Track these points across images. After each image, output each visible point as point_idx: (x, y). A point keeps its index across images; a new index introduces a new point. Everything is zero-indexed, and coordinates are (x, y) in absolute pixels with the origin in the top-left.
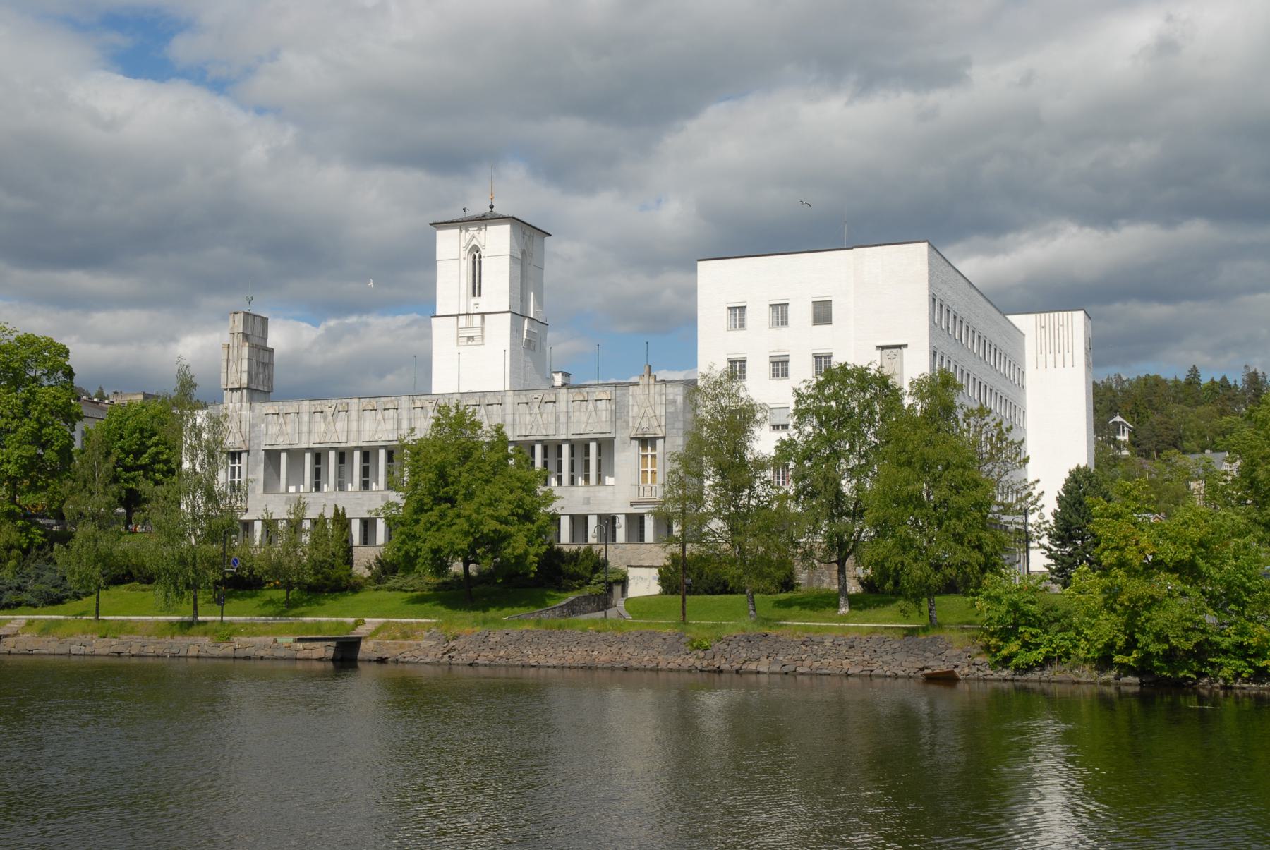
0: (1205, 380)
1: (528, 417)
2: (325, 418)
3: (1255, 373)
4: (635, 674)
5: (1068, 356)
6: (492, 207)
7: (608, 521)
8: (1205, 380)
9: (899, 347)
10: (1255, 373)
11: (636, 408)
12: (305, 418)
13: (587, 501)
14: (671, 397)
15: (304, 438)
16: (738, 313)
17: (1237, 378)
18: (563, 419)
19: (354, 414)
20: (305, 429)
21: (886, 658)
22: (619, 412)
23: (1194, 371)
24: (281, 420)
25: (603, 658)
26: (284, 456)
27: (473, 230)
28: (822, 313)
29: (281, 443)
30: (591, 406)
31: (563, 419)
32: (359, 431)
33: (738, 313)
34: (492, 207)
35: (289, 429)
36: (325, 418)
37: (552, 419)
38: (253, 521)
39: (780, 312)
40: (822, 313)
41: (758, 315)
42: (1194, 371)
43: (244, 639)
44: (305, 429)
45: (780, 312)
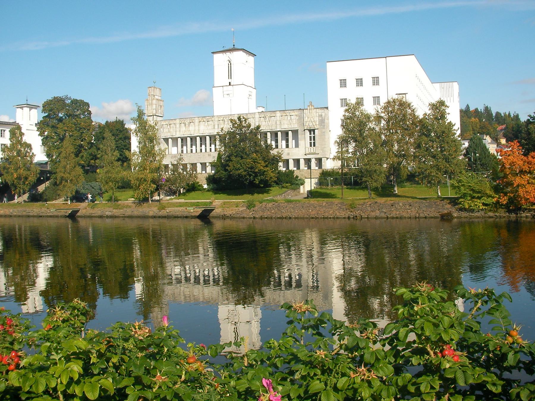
0: (472, 109)
1: (264, 123)
2: (185, 125)
3: (487, 107)
4: (32, 218)
5: (452, 98)
6: (234, 46)
7: (297, 162)
8: (472, 109)
9: (405, 94)
10: (487, 107)
11: (307, 118)
12: (178, 126)
13: (288, 154)
14: (320, 114)
15: (178, 133)
16: (343, 83)
17: (481, 108)
18: (278, 123)
19: (197, 123)
20: (178, 130)
21: (424, 209)
22: (301, 119)
23: (468, 106)
24: (169, 127)
25: (313, 213)
26: (170, 140)
27: (228, 54)
28: (376, 81)
29: (168, 135)
30: (289, 118)
31: (278, 123)
32: (199, 130)
33: (343, 83)
34: (234, 46)
35: (171, 130)
36: (185, 125)
37: (274, 123)
38: (196, 164)
39: (360, 82)
40: (376, 81)
41: (351, 83)
42: (468, 106)
43: (170, 209)
44: (178, 130)
45: (360, 82)
